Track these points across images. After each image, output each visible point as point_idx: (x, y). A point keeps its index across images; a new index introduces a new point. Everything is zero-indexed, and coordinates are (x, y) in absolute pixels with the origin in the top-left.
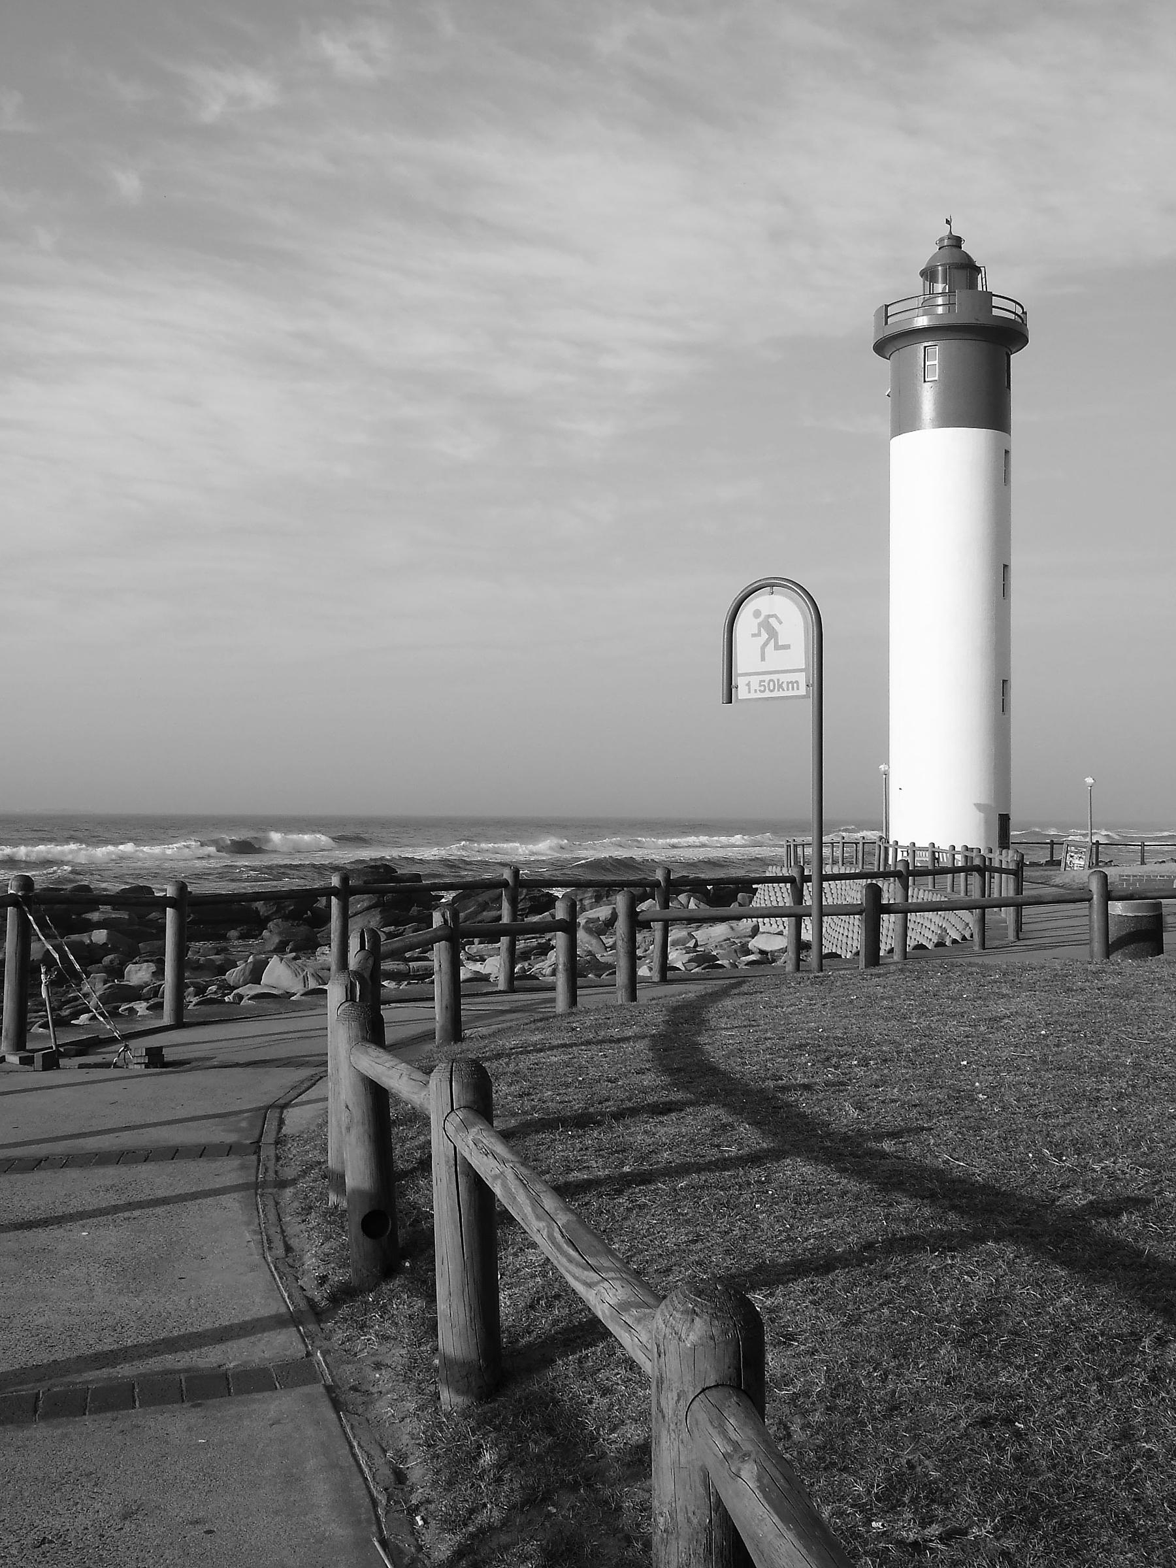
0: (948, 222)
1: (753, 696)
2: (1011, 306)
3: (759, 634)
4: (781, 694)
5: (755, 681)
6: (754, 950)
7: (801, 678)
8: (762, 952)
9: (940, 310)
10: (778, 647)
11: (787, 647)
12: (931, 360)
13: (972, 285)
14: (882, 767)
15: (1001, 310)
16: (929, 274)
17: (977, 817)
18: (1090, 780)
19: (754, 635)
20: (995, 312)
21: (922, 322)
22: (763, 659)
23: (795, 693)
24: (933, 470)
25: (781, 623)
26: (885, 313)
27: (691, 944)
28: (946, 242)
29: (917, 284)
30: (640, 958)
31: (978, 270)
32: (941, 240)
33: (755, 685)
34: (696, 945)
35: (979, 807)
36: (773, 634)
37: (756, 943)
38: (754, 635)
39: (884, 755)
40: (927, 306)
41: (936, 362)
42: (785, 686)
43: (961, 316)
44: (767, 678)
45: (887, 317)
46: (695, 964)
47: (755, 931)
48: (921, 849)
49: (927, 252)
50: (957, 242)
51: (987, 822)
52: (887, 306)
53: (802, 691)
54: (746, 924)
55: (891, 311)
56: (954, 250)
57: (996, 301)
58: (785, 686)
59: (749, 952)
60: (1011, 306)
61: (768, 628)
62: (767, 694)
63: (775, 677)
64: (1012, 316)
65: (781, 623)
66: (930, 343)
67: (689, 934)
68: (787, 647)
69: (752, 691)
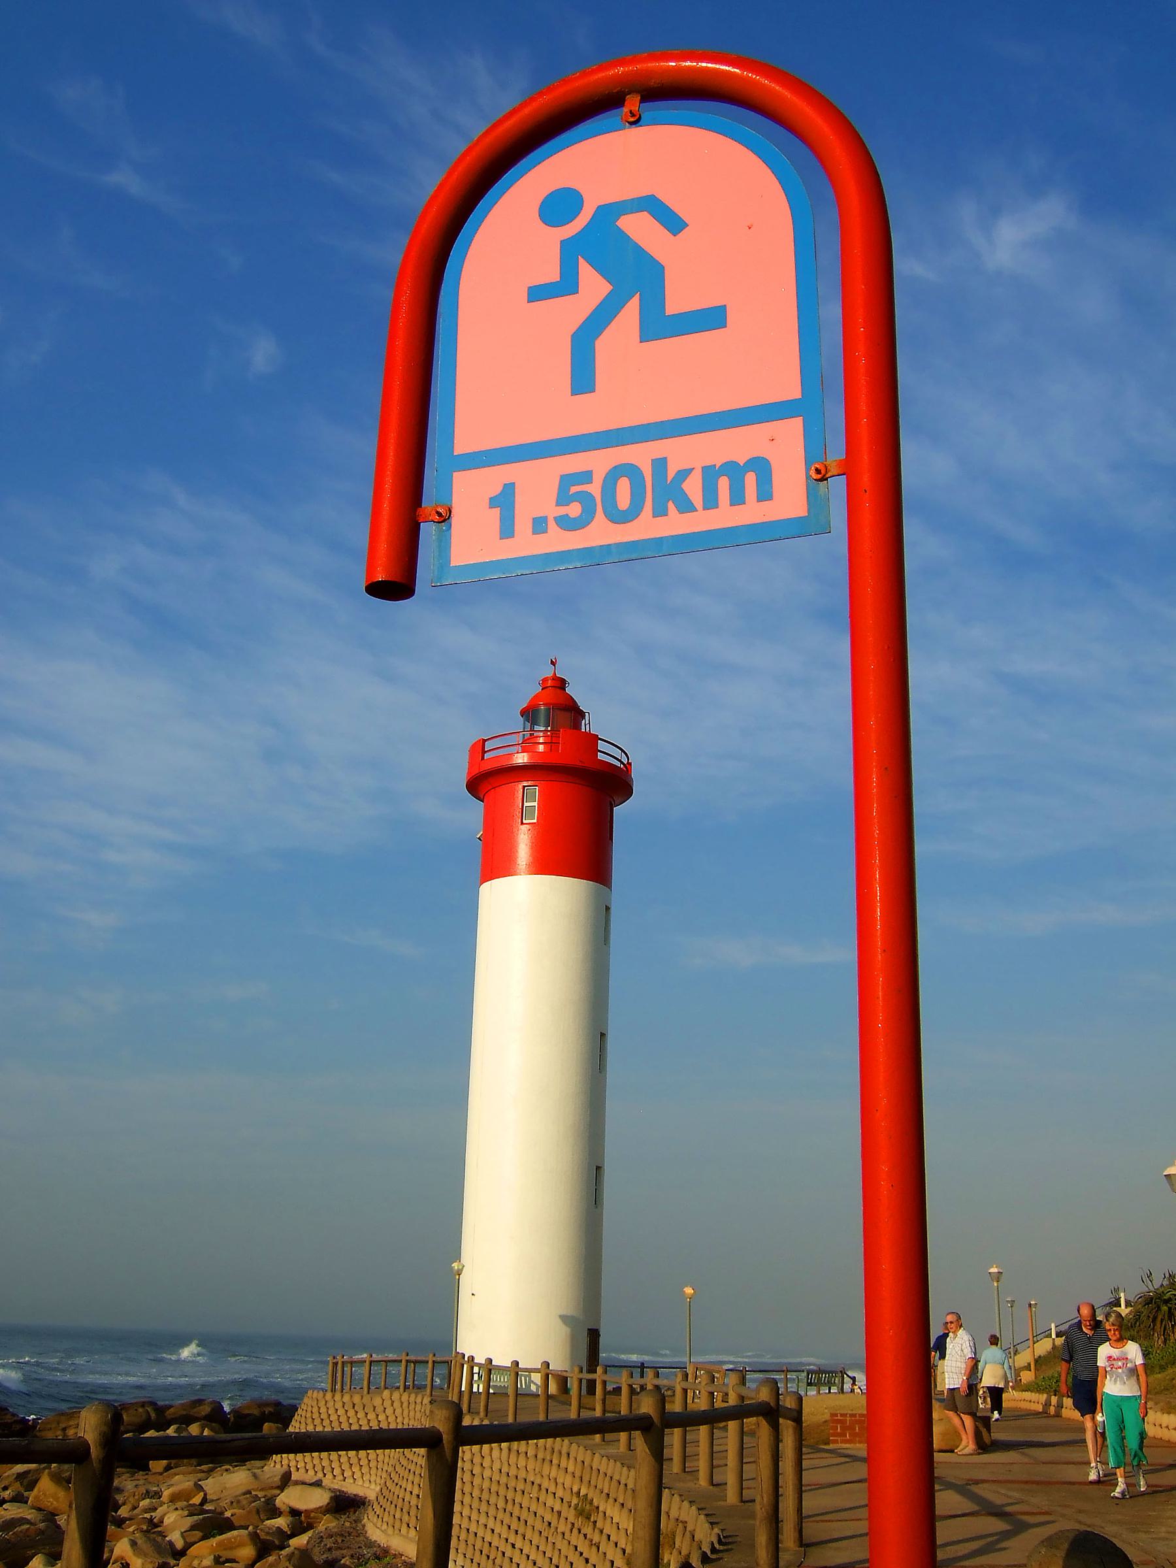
0: (553, 663)
1: (526, 545)
2: (617, 753)
3: (567, 285)
4: (676, 524)
5: (536, 486)
6: (283, 1508)
7: (786, 448)
8: (295, 1513)
9: (541, 748)
10: (659, 325)
11: (712, 319)
12: (528, 800)
13: (577, 726)
14: (455, 1265)
15: (606, 754)
16: (529, 714)
17: (563, 1331)
18: (689, 1291)
19: (537, 294)
20: (600, 756)
21: (522, 759)
22: (583, 379)
23: (752, 513)
24: (524, 924)
25: (673, 223)
26: (479, 748)
27: (197, 1500)
28: (549, 683)
29: (519, 723)
30: (120, 1523)
31: (582, 714)
32: (545, 680)
33: (536, 486)
34: (204, 1501)
35: (564, 1319)
36: (638, 277)
37: (289, 1498)
38: (537, 294)
39: (455, 1252)
40: (528, 744)
41: (536, 804)
42: (693, 487)
43: (567, 755)
44: (599, 462)
45: (484, 752)
46: (199, 1534)
47: (286, 1480)
48: (499, 1368)
49: (530, 690)
50: (561, 684)
51: (573, 1338)
52: (484, 741)
53: (790, 498)
54: (277, 1464)
55: (488, 746)
56: (559, 691)
57: (601, 746)
58: (693, 487)
59: (275, 1512)
60: (617, 753)
61: (613, 258)
62: (601, 533)
63: (641, 455)
64: (618, 764)
65: (673, 223)
66: (530, 783)
67: (196, 1484)
68: (712, 319)
69: (523, 525)
